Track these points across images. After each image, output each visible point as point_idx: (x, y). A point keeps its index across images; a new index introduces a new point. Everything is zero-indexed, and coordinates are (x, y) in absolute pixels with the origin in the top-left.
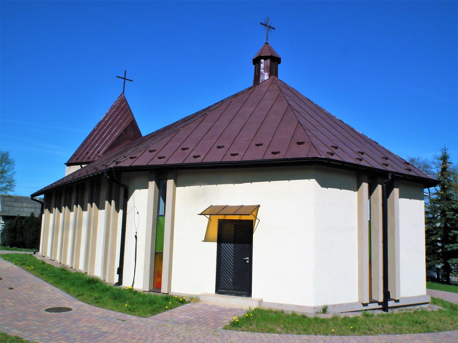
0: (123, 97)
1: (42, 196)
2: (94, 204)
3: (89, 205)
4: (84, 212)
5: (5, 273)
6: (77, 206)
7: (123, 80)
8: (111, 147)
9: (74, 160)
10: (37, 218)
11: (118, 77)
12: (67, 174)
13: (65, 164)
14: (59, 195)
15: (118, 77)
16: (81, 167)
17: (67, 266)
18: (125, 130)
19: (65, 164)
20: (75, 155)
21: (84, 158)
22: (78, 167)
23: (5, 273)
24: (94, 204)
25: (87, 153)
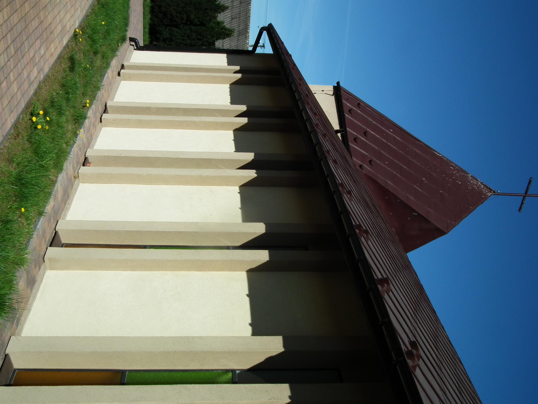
0: (485, 195)
1: (268, 50)
2: (239, 76)
3: (238, 68)
4: (230, 135)
5: (26, 85)
6: (236, 72)
7: (527, 198)
8: (383, 192)
9: (347, 104)
10: (215, 18)
11: (530, 181)
12: (314, 88)
13: (338, 83)
14: (270, 88)
15: (530, 181)
16: (337, 132)
17: (113, 89)
18: (422, 218)
19: (338, 83)
20: (359, 104)
21: (355, 127)
22: (336, 126)
23: (26, 85)
24: (239, 76)
25: (365, 133)
